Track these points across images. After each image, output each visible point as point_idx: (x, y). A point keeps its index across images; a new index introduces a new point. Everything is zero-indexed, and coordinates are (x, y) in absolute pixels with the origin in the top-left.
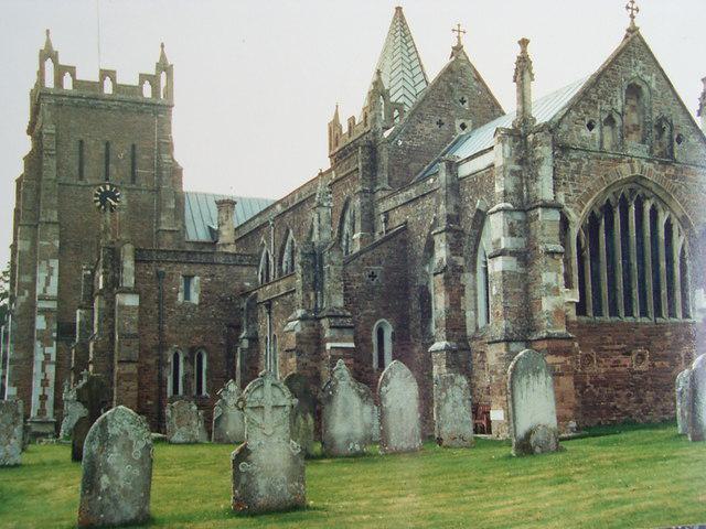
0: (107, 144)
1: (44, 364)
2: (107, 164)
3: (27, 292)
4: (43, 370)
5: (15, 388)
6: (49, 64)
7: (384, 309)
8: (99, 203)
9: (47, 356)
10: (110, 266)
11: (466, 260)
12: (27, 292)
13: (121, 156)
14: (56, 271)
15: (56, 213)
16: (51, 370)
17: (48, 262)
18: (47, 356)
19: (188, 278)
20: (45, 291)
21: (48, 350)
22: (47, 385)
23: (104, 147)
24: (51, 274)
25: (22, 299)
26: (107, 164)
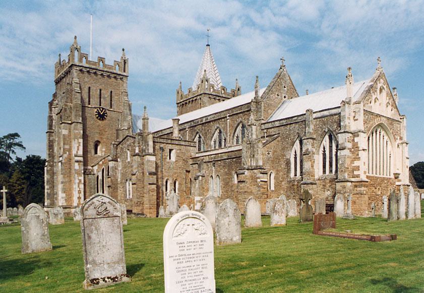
0: (100, 90)
1: (79, 184)
2: (100, 98)
3: (67, 153)
4: (79, 187)
5: (65, 194)
6: (76, 53)
7: (272, 167)
8: (97, 116)
9: (80, 181)
10: (141, 143)
11: (316, 149)
12: (67, 153)
13: (106, 96)
14: (82, 144)
15: (81, 118)
16: (82, 186)
17: (78, 140)
18: (80, 181)
19: (171, 150)
20: (77, 152)
21: (80, 178)
22: (80, 193)
23: (99, 91)
24: (80, 145)
25: (65, 156)
26: (100, 98)
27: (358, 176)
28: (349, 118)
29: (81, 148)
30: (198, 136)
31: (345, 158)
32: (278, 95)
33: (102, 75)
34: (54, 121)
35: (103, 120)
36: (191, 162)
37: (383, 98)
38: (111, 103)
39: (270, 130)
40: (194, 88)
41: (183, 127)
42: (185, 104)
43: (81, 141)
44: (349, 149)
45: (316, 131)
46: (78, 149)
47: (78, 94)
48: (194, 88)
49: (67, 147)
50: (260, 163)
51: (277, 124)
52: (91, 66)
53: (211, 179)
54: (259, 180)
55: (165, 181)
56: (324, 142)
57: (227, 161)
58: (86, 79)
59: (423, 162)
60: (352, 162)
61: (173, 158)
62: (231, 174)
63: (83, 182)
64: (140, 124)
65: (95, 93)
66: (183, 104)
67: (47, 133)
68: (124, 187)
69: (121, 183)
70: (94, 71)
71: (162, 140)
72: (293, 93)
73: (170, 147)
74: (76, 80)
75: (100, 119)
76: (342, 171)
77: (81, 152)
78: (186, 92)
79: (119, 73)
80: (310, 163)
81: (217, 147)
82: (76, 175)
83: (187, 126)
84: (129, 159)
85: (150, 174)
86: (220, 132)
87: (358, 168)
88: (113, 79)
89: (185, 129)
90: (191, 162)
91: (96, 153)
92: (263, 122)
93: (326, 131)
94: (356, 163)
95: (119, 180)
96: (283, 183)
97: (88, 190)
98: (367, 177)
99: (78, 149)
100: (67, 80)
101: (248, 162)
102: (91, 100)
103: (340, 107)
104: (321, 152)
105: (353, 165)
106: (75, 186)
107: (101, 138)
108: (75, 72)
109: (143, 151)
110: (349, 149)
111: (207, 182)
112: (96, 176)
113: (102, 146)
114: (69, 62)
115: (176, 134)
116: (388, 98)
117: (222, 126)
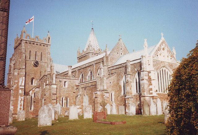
2: (36, 56)
9: (22, 99)
16: (22, 102)
19: (65, 82)
21: (22, 98)
23: (35, 52)
26: (36, 56)
27: (152, 93)
28: (146, 64)
29: (24, 82)
30: (81, 74)
31: (144, 84)
32: (118, 53)
33: (37, 44)
34: (12, 68)
35: (36, 67)
36: (75, 88)
37: (165, 53)
38: (41, 59)
39: (112, 71)
40: (85, 50)
41: (74, 70)
42: (81, 58)
43: (24, 78)
44: (146, 79)
45: (132, 70)
46: (22, 82)
47: (24, 54)
48: (85, 50)
49: (17, 81)
50: (105, 88)
51: (115, 68)
52: (31, 40)
53: (84, 96)
54: (104, 96)
55: (62, 98)
56: (136, 76)
57: (91, 87)
58: (29, 47)
59: (89, 119)
60: (149, 86)
61: (66, 86)
62: (93, 94)
63: (23, 100)
64: (49, 69)
65: (33, 54)
66: (80, 58)
67: (8, 74)
68: (42, 102)
69: (41, 99)
70: (33, 43)
71: (61, 77)
72: (126, 52)
73: (65, 80)
74: (24, 47)
75: (35, 67)
76: (143, 91)
77: (23, 84)
78: (81, 52)
79: (46, 43)
80: (129, 87)
81: (90, 80)
82: (20, 96)
83: (77, 69)
84: (44, 87)
85: (53, 94)
86: (91, 72)
87: (151, 89)
88: (43, 47)
89: (76, 71)
90: (75, 88)
91: (32, 84)
92: (109, 67)
93: (136, 70)
94: (151, 87)
95: (40, 98)
96: (118, 98)
97: (26, 104)
98: (159, 94)
99: (22, 82)
100: (19, 47)
101: (99, 87)
102: (31, 57)
103: (141, 59)
104: (135, 82)
105: (149, 88)
106: (19, 102)
107: (35, 76)
108: (23, 44)
109: (51, 82)
110: (146, 79)
111: (82, 98)
112: (30, 96)
113: (35, 81)
114: (20, 39)
115: (70, 73)
116: (168, 53)
117: (91, 69)
